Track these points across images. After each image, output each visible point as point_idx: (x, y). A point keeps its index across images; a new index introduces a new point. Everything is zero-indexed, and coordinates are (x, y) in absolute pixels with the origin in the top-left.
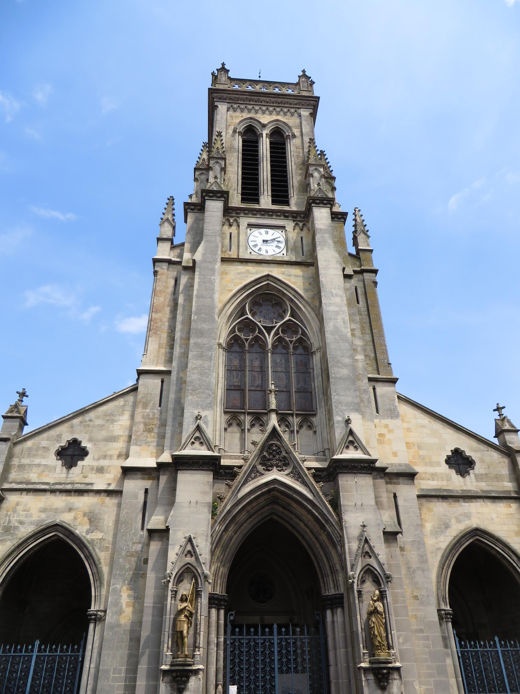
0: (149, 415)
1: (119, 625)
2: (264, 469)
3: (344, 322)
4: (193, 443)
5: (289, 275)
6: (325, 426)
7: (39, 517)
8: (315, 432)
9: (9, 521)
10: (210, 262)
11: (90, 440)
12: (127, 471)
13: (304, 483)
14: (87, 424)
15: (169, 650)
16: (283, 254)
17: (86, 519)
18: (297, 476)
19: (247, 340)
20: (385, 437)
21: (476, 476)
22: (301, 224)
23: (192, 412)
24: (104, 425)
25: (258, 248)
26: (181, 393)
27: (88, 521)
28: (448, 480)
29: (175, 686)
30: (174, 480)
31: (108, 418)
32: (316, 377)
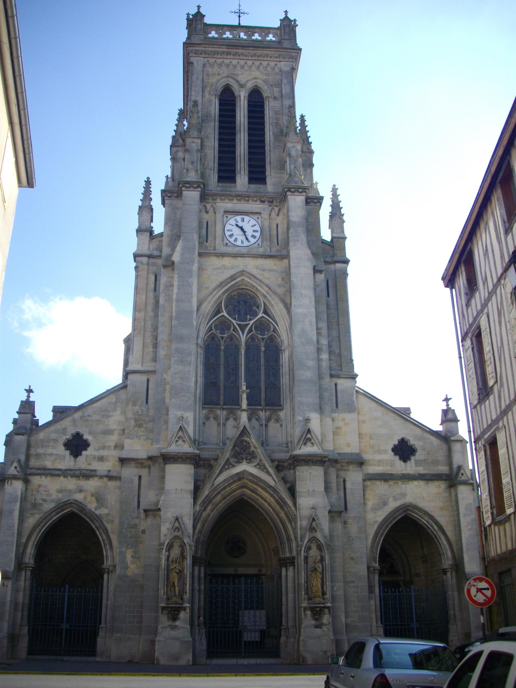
0: (139, 412)
1: (126, 576)
2: (235, 461)
3: (311, 324)
4: (177, 441)
5: (263, 270)
6: (290, 421)
7: (57, 496)
8: (281, 425)
9: (35, 499)
10: (188, 263)
11: (90, 433)
12: (123, 461)
13: (268, 473)
14: (86, 418)
15: (165, 594)
16: (258, 245)
17: (94, 498)
18: (262, 467)
19: (222, 338)
20: (341, 430)
21: (415, 460)
22: (276, 209)
23: (176, 414)
24: (100, 420)
25: (233, 239)
26: (165, 393)
27: (95, 500)
28: (391, 466)
29: (171, 617)
30: (163, 470)
31: (103, 414)
32: (284, 374)
